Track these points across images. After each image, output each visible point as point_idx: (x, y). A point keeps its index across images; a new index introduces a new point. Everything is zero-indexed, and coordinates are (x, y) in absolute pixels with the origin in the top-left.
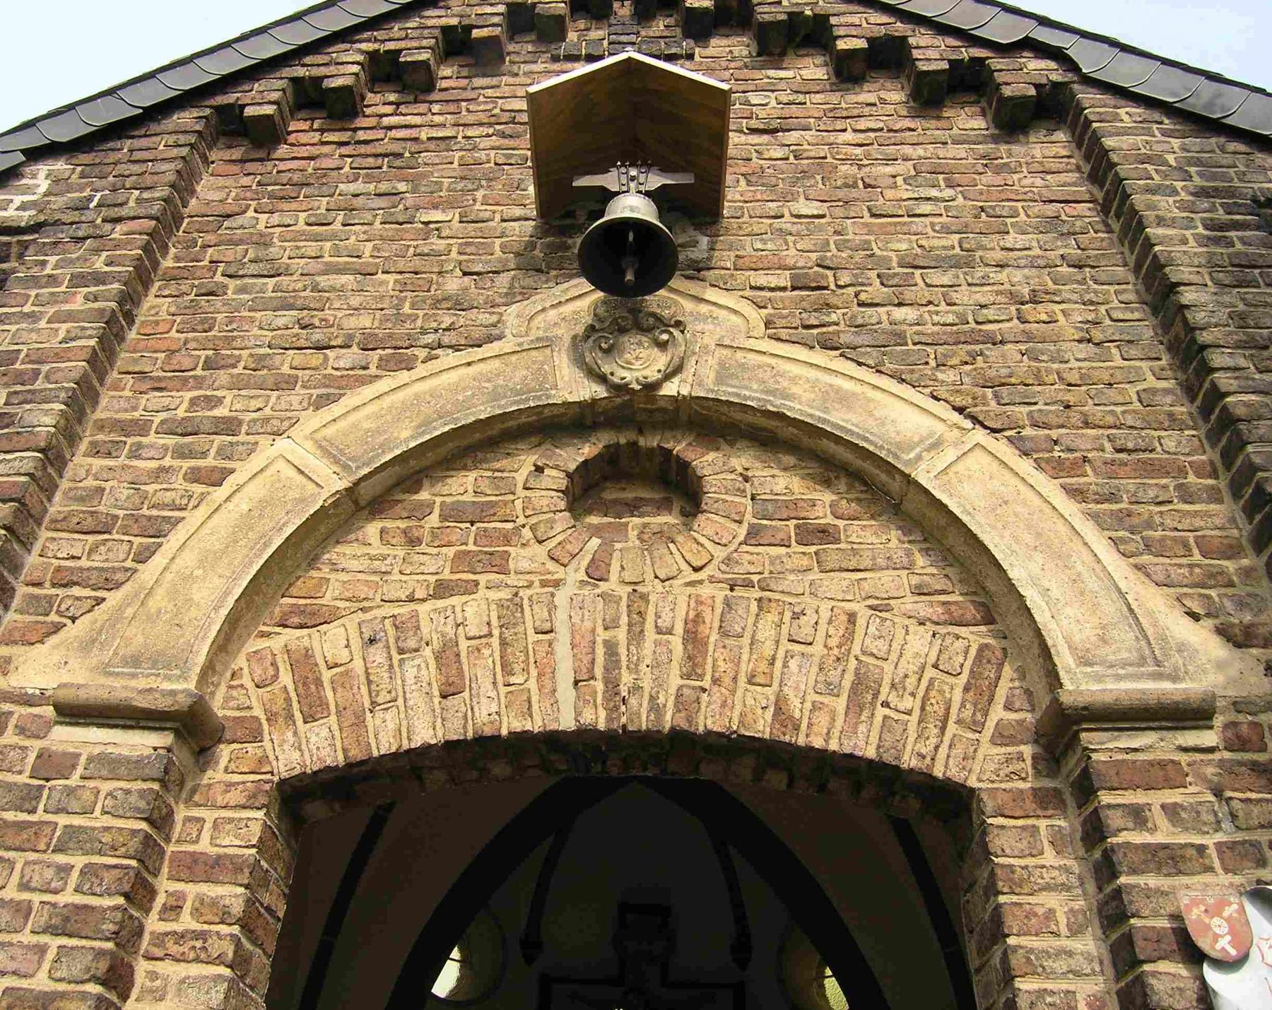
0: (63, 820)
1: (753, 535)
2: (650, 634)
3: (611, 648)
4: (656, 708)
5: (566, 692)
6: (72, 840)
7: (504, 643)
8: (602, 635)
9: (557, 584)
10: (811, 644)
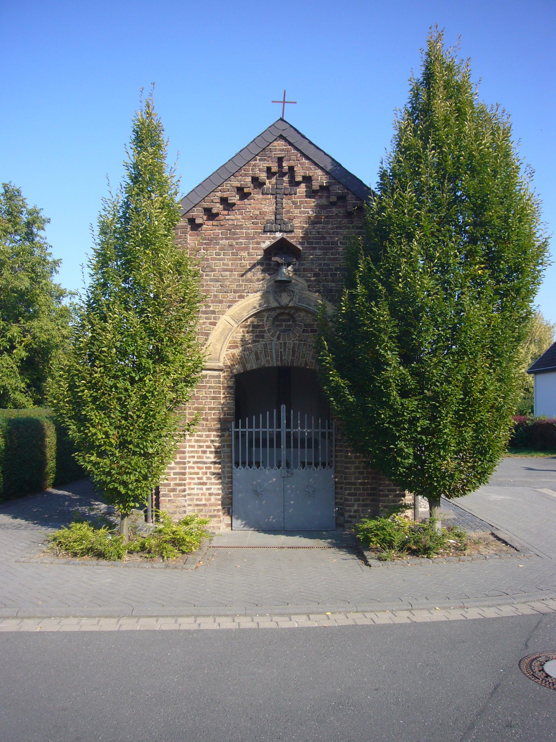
0: (208, 385)
1: (304, 331)
2: (287, 350)
3: (281, 352)
4: (288, 363)
5: (275, 360)
6: (210, 387)
7: (265, 352)
8: (280, 350)
9: (272, 341)
10: (281, 137)
